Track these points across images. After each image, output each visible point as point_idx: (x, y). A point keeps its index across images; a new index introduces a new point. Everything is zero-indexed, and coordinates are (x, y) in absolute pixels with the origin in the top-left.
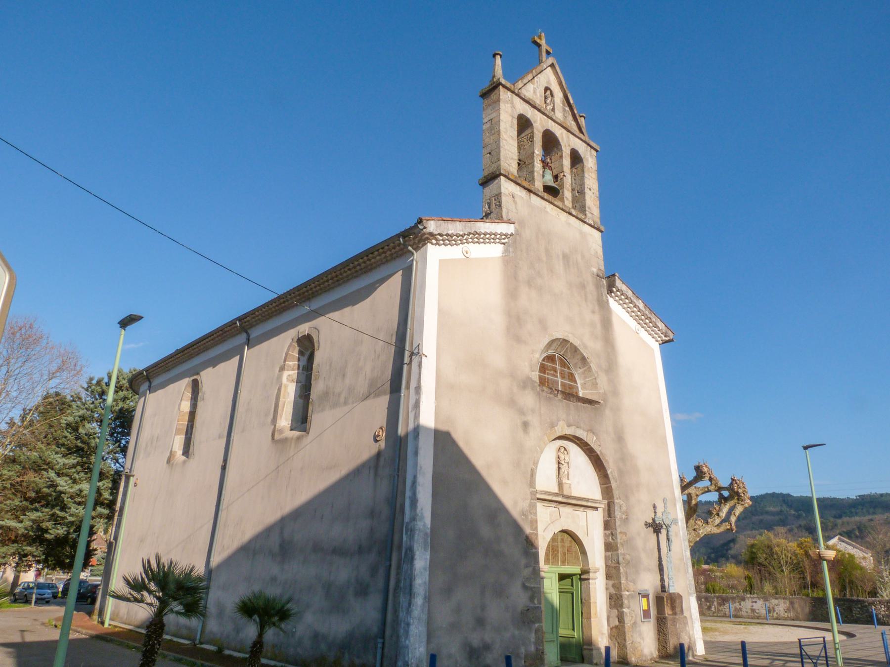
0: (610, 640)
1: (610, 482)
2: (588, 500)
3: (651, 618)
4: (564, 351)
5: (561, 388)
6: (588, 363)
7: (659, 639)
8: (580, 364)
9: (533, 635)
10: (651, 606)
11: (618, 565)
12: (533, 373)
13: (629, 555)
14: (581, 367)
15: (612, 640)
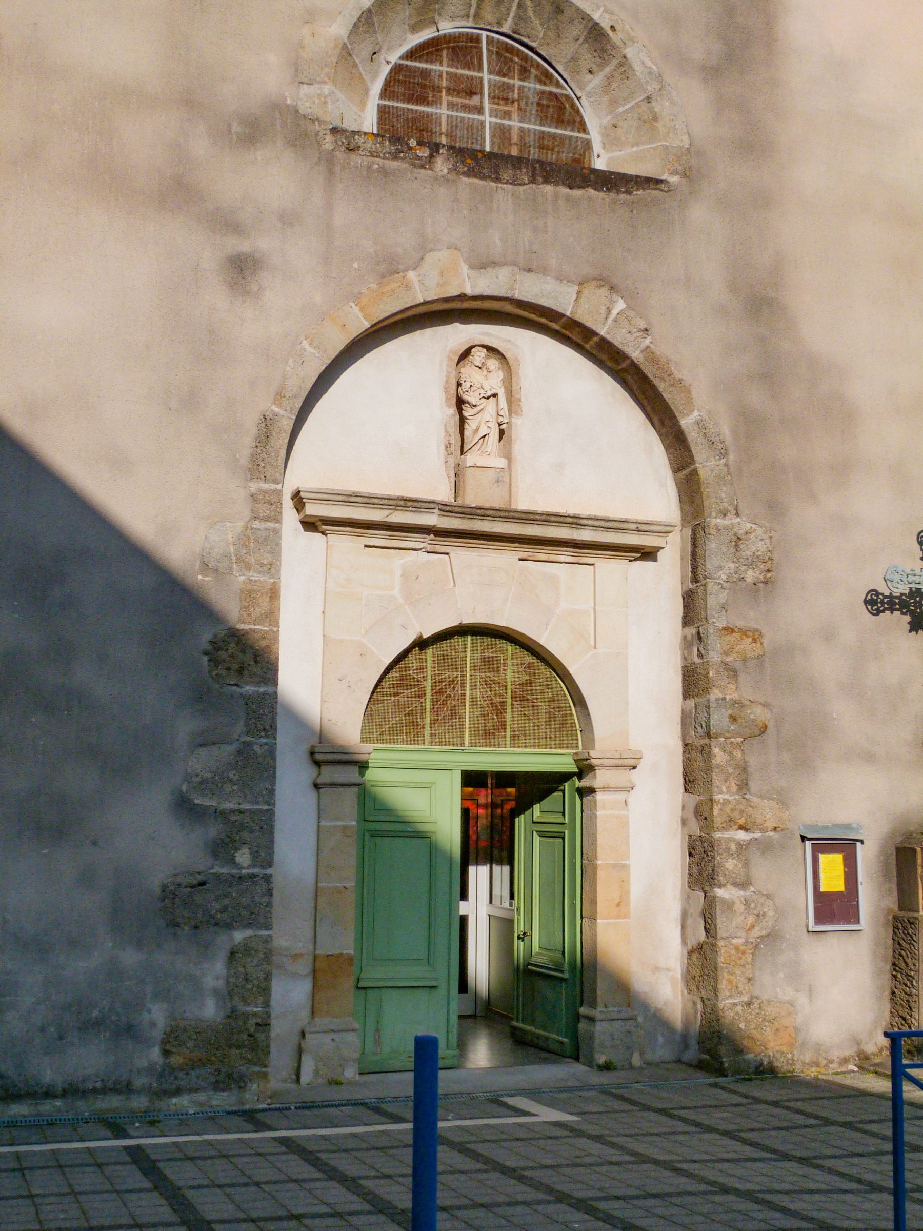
0: (685, 992)
1: (692, 457)
2: (576, 521)
3: (858, 921)
4: (512, 14)
5: (492, 146)
6: (614, 47)
7: (893, 993)
8: (587, 59)
9: (220, 967)
10: (861, 877)
11: (707, 741)
12: (305, 89)
13: (765, 705)
14: (595, 68)
15: (690, 991)
